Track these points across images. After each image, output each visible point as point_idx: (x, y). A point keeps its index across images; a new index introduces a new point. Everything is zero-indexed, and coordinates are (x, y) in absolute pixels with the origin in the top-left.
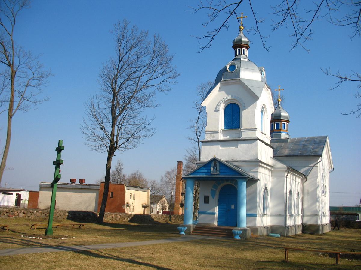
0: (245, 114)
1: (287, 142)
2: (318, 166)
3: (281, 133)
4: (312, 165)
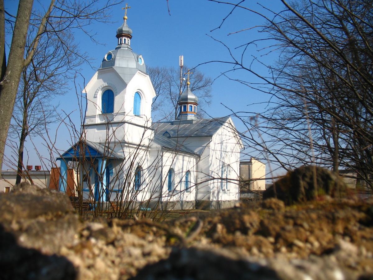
0: (117, 99)
1: (192, 123)
2: (210, 146)
3: (187, 115)
4: (205, 145)
